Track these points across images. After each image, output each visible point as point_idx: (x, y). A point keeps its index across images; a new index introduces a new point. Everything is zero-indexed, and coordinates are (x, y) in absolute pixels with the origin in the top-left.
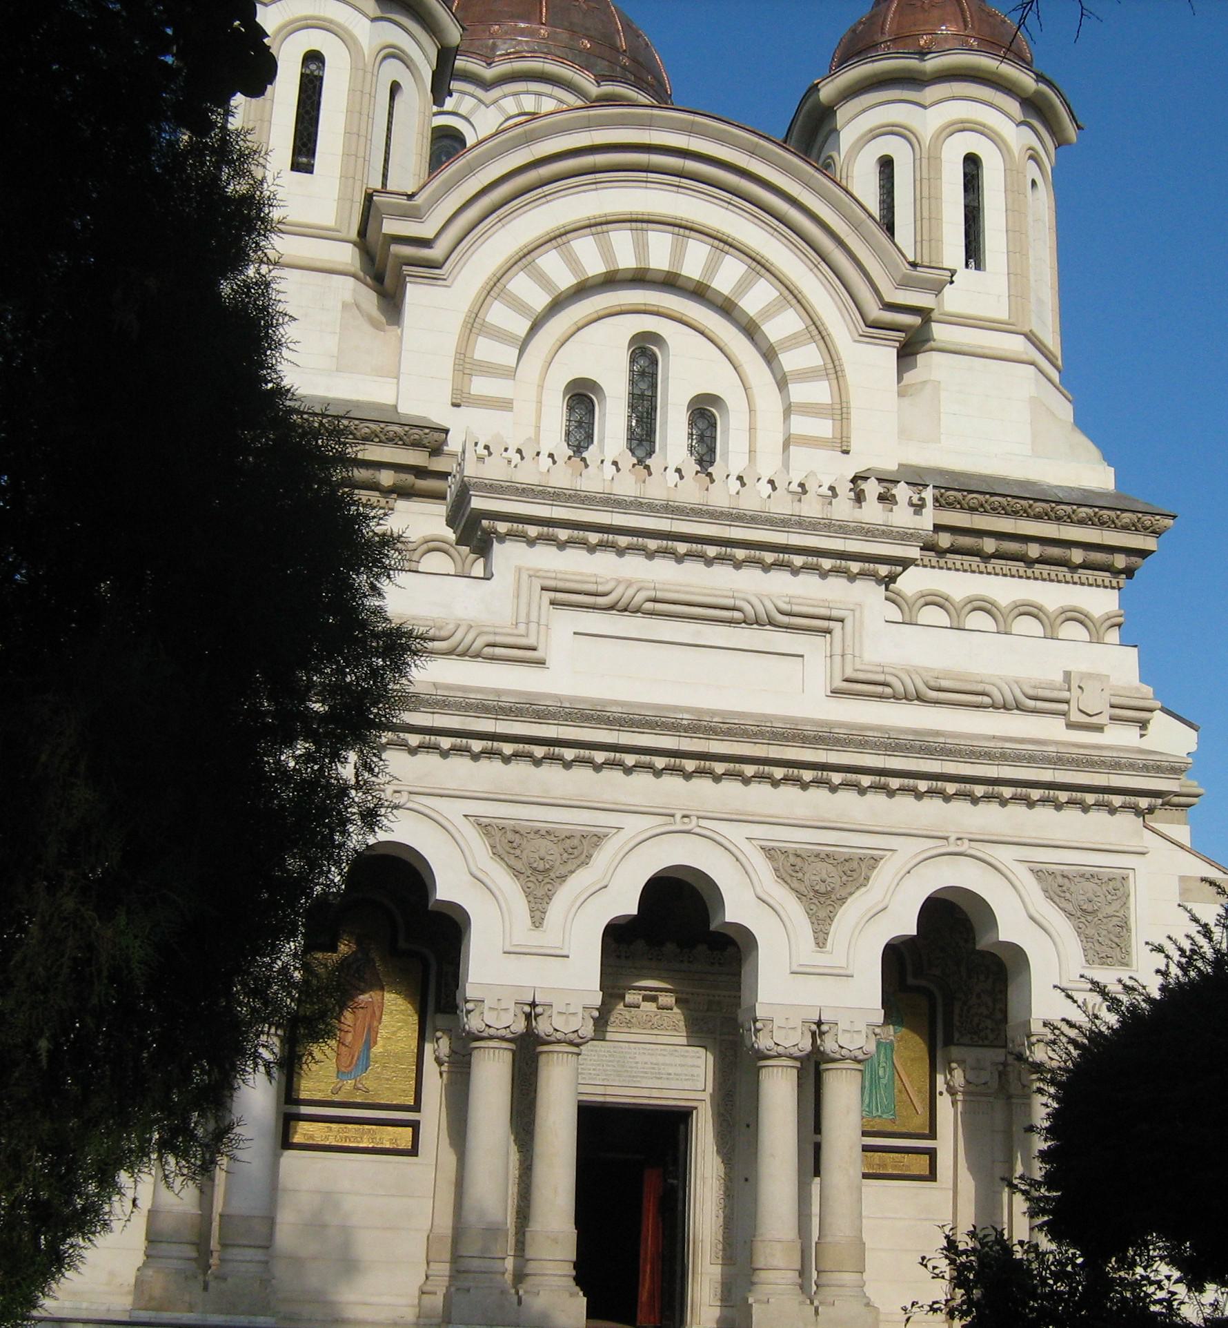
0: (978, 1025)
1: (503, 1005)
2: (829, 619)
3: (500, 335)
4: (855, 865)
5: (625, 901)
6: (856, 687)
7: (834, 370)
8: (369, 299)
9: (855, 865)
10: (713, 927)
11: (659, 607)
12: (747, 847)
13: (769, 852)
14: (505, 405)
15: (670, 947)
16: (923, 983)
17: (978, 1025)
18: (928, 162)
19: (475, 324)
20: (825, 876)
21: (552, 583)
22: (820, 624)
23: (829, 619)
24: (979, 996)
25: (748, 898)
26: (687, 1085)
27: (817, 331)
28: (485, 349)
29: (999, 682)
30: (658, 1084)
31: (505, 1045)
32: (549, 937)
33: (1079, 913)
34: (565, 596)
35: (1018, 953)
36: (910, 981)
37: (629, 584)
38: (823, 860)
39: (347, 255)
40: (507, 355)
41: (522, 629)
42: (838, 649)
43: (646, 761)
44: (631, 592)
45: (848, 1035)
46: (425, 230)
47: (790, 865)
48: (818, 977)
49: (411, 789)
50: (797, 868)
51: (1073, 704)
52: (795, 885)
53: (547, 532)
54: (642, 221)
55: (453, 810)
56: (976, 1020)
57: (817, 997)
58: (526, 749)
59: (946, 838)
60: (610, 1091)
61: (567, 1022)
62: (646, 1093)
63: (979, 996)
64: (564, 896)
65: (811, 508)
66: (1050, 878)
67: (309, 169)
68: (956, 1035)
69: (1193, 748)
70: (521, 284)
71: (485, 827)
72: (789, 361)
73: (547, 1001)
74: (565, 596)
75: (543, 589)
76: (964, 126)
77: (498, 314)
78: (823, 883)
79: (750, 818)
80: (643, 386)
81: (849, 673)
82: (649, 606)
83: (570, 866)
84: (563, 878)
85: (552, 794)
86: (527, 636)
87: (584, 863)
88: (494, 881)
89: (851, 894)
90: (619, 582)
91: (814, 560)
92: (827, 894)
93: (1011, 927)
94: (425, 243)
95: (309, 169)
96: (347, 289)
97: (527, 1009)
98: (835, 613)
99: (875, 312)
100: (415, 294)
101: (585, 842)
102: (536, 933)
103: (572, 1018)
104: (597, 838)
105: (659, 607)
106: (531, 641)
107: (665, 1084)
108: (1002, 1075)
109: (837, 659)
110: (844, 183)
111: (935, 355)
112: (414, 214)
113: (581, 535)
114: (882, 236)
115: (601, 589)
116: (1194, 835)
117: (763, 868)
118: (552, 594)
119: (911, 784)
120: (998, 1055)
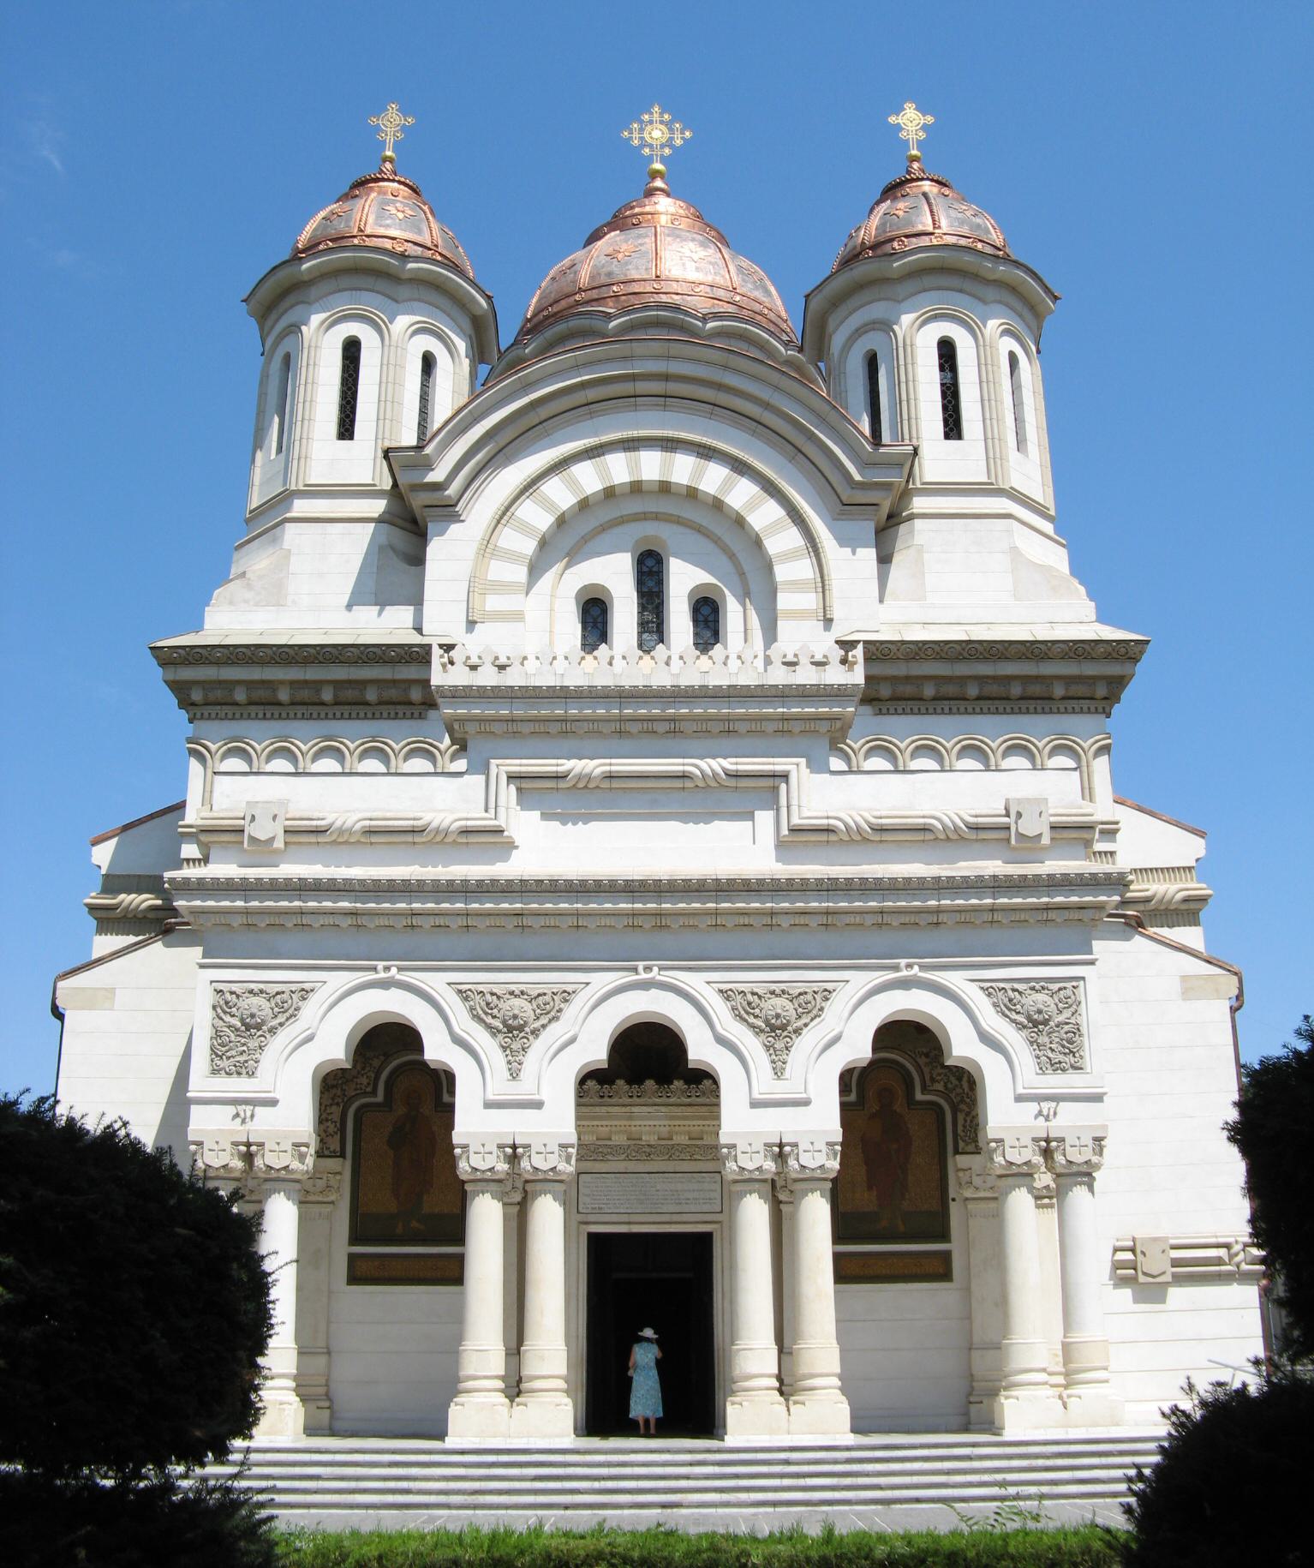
1: (487, 1149)
4: (809, 997)
5: (596, 1052)
9: (809, 997)
10: (348, 1066)
14: (518, 616)
26: (706, 1208)
29: (938, 814)
32: (523, 1089)
36: (919, 1096)
48: (782, 1102)
57: (777, 1124)
64: (806, 1043)
65: (806, 676)
66: (1000, 994)
68: (961, 1144)
69: (1202, 853)
73: (465, 1142)
80: (651, 584)
82: (605, 784)
89: (806, 1025)
93: (962, 1046)
94: (437, 487)
97: (243, 1149)
111: (918, 523)
116: (1208, 941)
117: (720, 1010)
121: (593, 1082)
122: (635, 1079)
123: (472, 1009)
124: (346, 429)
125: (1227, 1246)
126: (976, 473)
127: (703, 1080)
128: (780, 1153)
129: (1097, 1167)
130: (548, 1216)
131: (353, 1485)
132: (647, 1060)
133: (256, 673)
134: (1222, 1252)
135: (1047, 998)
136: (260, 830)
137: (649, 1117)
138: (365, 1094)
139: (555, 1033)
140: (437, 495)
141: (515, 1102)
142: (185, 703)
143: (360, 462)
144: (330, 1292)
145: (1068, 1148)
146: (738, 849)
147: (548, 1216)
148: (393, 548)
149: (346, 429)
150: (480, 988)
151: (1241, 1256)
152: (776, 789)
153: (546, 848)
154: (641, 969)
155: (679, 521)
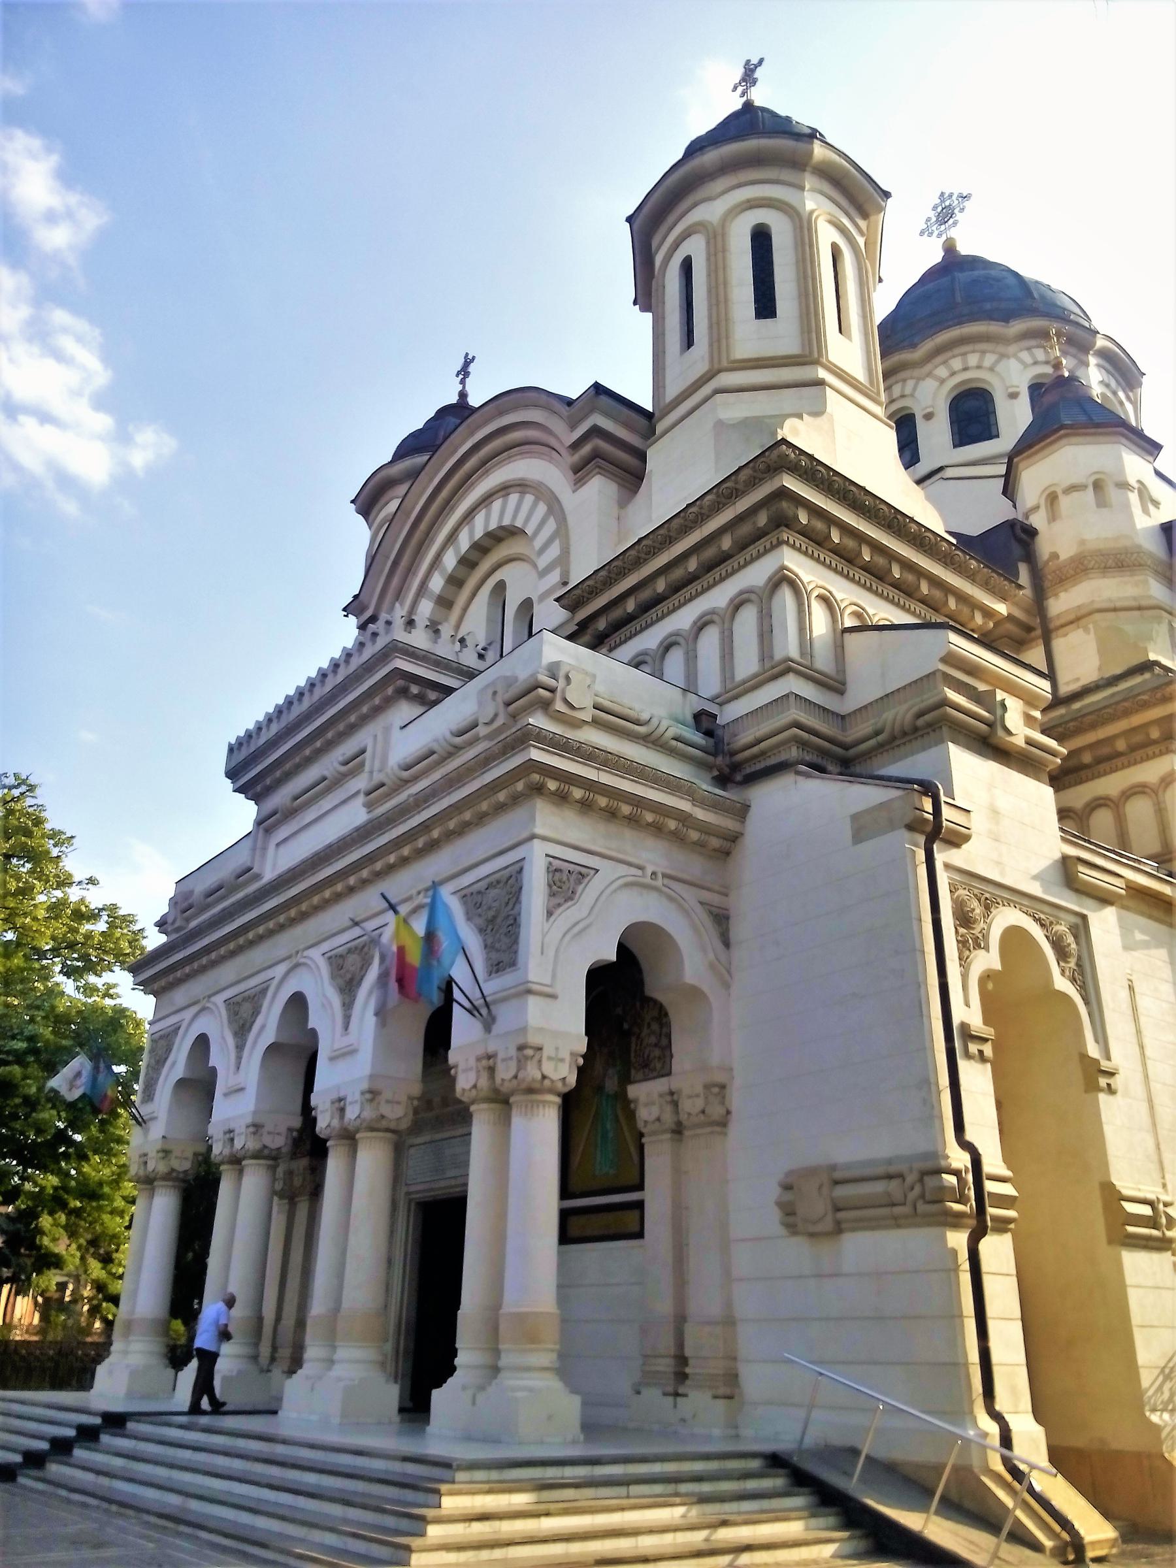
103: (560, 1065)
125: (900, 1176)
134: (894, 1185)
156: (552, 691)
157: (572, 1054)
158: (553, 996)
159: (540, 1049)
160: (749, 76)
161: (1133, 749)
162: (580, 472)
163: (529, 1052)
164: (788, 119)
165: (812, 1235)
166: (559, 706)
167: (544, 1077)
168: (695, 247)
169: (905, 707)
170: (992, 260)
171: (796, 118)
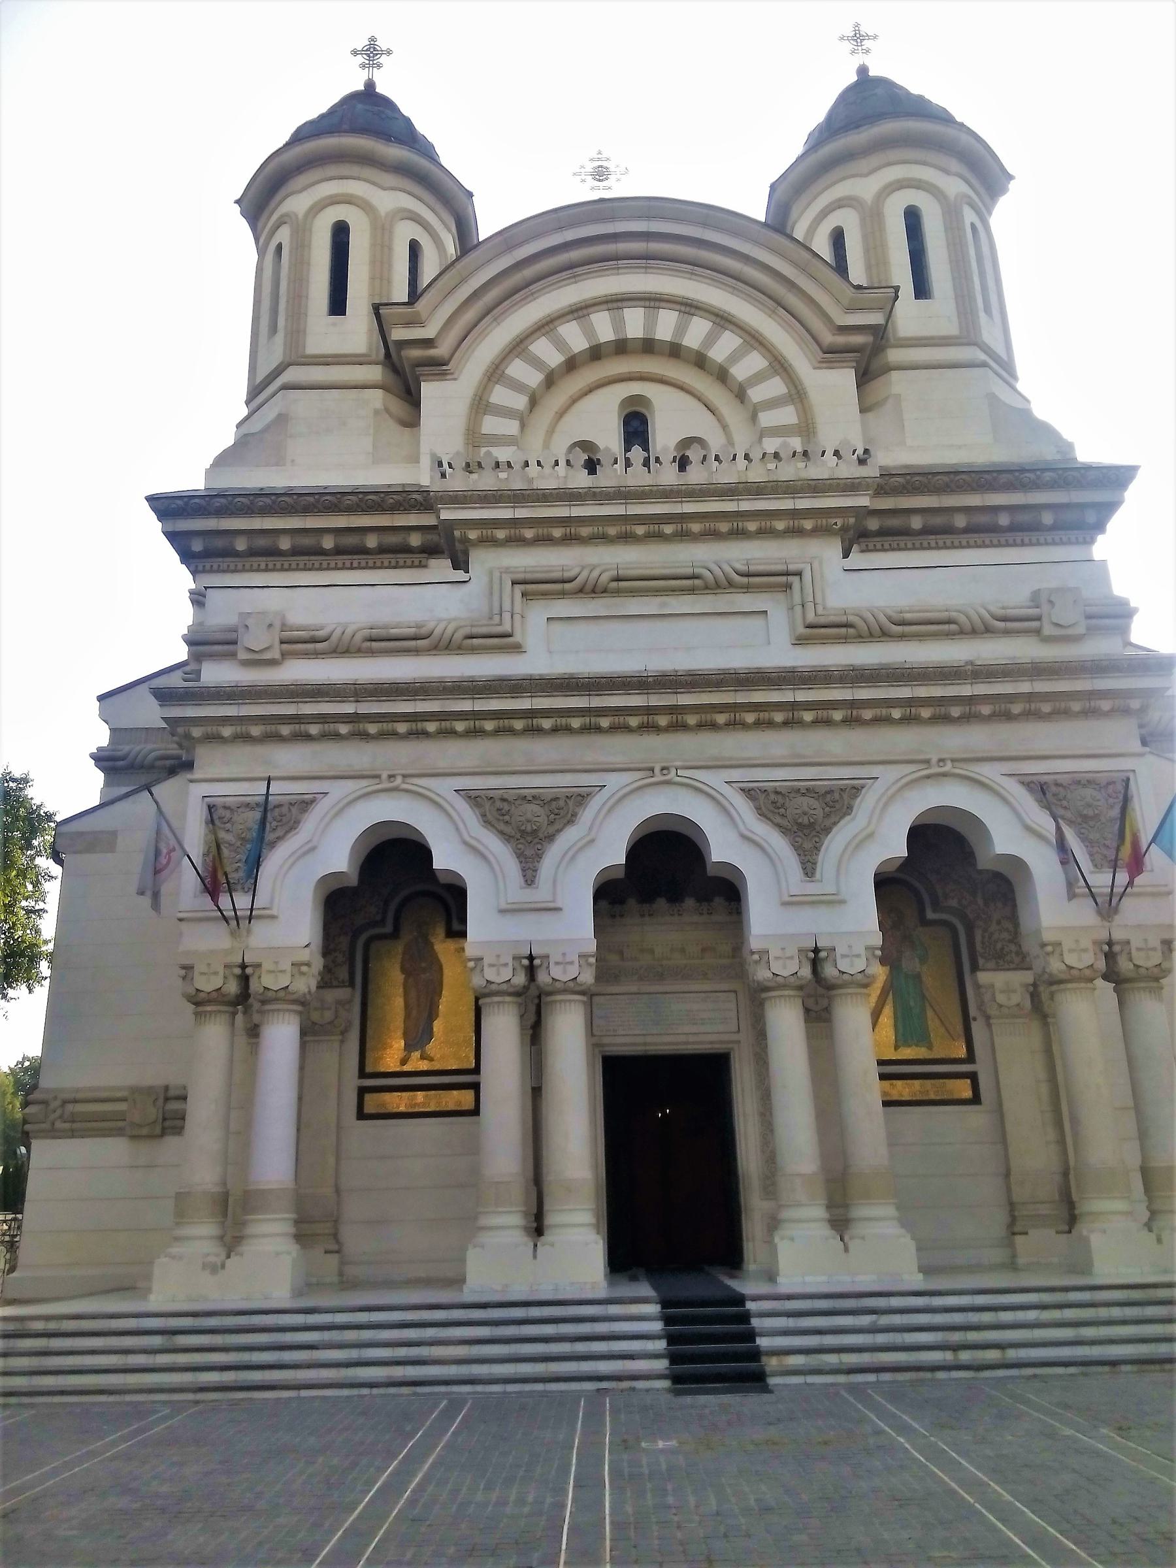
0: (1002, 949)
1: (502, 961)
2: (787, 574)
3: (506, 412)
6: (818, 631)
7: (797, 395)
8: (398, 406)
11: (621, 585)
12: (727, 790)
13: (748, 793)
15: (690, 902)
16: (944, 916)
17: (1002, 949)
18: (873, 218)
19: (480, 406)
20: (806, 809)
21: (520, 576)
22: (782, 581)
23: (787, 574)
24: (999, 923)
25: (731, 839)
27: (779, 365)
28: (491, 425)
30: (694, 1029)
31: (508, 999)
32: (541, 893)
33: (1079, 820)
34: (534, 587)
35: (1017, 863)
36: (930, 915)
37: (593, 568)
38: (803, 795)
39: (375, 373)
40: (511, 427)
41: (497, 619)
42: (797, 598)
43: (620, 723)
44: (595, 574)
45: (847, 960)
46: (429, 332)
47: (771, 803)
48: (811, 907)
49: (404, 772)
50: (779, 805)
51: (1045, 619)
52: (778, 820)
53: (515, 535)
54: (617, 301)
55: (445, 787)
56: (999, 946)
58: (505, 725)
59: (927, 762)
60: (649, 1039)
61: (565, 972)
62: (682, 1038)
63: (999, 923)
67: (342, 312)
68: (981, 961)
70: (518, 369)
71: (473, 798)
72: (740, 372)
74: (534, 587)
75: (513, 583)
76: (348, 200)
77: (500, 395)
78: (806, 818)
79: (728, 763)
81: (811, 617)
82: (614, 584)
83: (557, 826)
84: (551, 838)
85: (534, 765)
86: (500, 624)
87: (571, 822)
88: (487, 848)
89: (835, 824)
90: (583, 568)
91: (766, 527)
92: (811, 825)
94: (428, 343)
95: (342, 312)
96: (376, 398)
98: (792, 567)
99: (829, 338)
100: (429, 390)
101: (571, 803)
102: (528, 891)
103: (569, 967)
104: (581, 798)
105: (621, 585)
106: (507, 627)
107: (702, 1029)
108: (1035, 996)
109: (798, 609)
110: (788, 231)
111: (895, 375)
112: (413, 322)
113: (544, 535)
114: (834, 278)
115: (567, 575)
117: (743, 808)
118: (522, 587)
119: (881, 716)
120: (1027, 977)
121: (611, 895)
122: (647, 896)
123: (484, 815)
124: (338, 305)
126: (949, 326)
127: (727, 891)
128: (816, 957)
129: (1168, 972)
130: (569, 1033)
131: (354, 1354)
132: (665, 873)
133: (341, 521)
135: (1095, 793)
136: (257, 639)
137: (667, 933)
138: (375, 924)
139: (570, 836)
140: (432, 352)
141: (531, 913)
142: (187, 557)
143: (355, 332)
144: (339, 1127)
145: (1134, 952)
146: (760, 640)
147: (569, 1033)
148: (387, 410)
149: (338, 305)
150: (491, 794)
151: (59, 1112)
152: (788, 587)
153: (554, 645)
154: (657, 770)
155: (662, 381)
156: (1039, 618)
157: (1095, 943)
158: (273, 917)
159: (1128, 942)
160: (372, 53)
161: (926, 531)
162: (831, 355)
163: (1049, 949)
164: (921, 99)
165: (133, 1137)
166: (1048, 630)
167: (1137, 967)
168: (849, 221)
169: (150, 746)
170: (324, 109)
171: (929, 96)
